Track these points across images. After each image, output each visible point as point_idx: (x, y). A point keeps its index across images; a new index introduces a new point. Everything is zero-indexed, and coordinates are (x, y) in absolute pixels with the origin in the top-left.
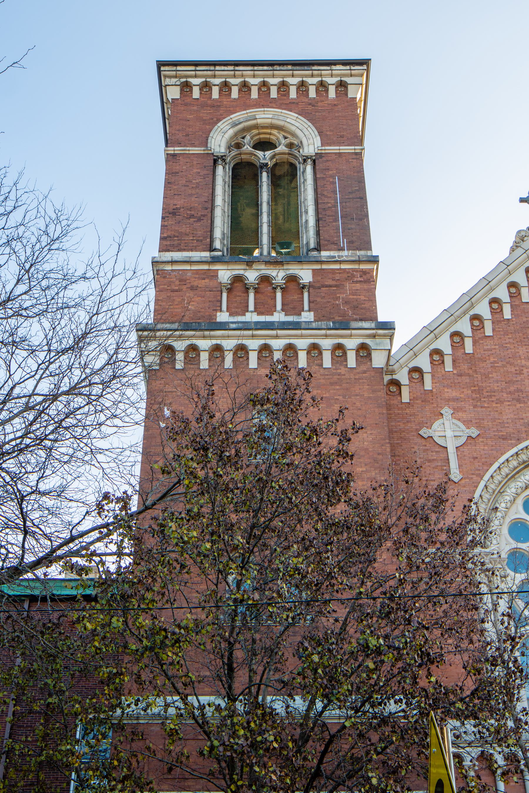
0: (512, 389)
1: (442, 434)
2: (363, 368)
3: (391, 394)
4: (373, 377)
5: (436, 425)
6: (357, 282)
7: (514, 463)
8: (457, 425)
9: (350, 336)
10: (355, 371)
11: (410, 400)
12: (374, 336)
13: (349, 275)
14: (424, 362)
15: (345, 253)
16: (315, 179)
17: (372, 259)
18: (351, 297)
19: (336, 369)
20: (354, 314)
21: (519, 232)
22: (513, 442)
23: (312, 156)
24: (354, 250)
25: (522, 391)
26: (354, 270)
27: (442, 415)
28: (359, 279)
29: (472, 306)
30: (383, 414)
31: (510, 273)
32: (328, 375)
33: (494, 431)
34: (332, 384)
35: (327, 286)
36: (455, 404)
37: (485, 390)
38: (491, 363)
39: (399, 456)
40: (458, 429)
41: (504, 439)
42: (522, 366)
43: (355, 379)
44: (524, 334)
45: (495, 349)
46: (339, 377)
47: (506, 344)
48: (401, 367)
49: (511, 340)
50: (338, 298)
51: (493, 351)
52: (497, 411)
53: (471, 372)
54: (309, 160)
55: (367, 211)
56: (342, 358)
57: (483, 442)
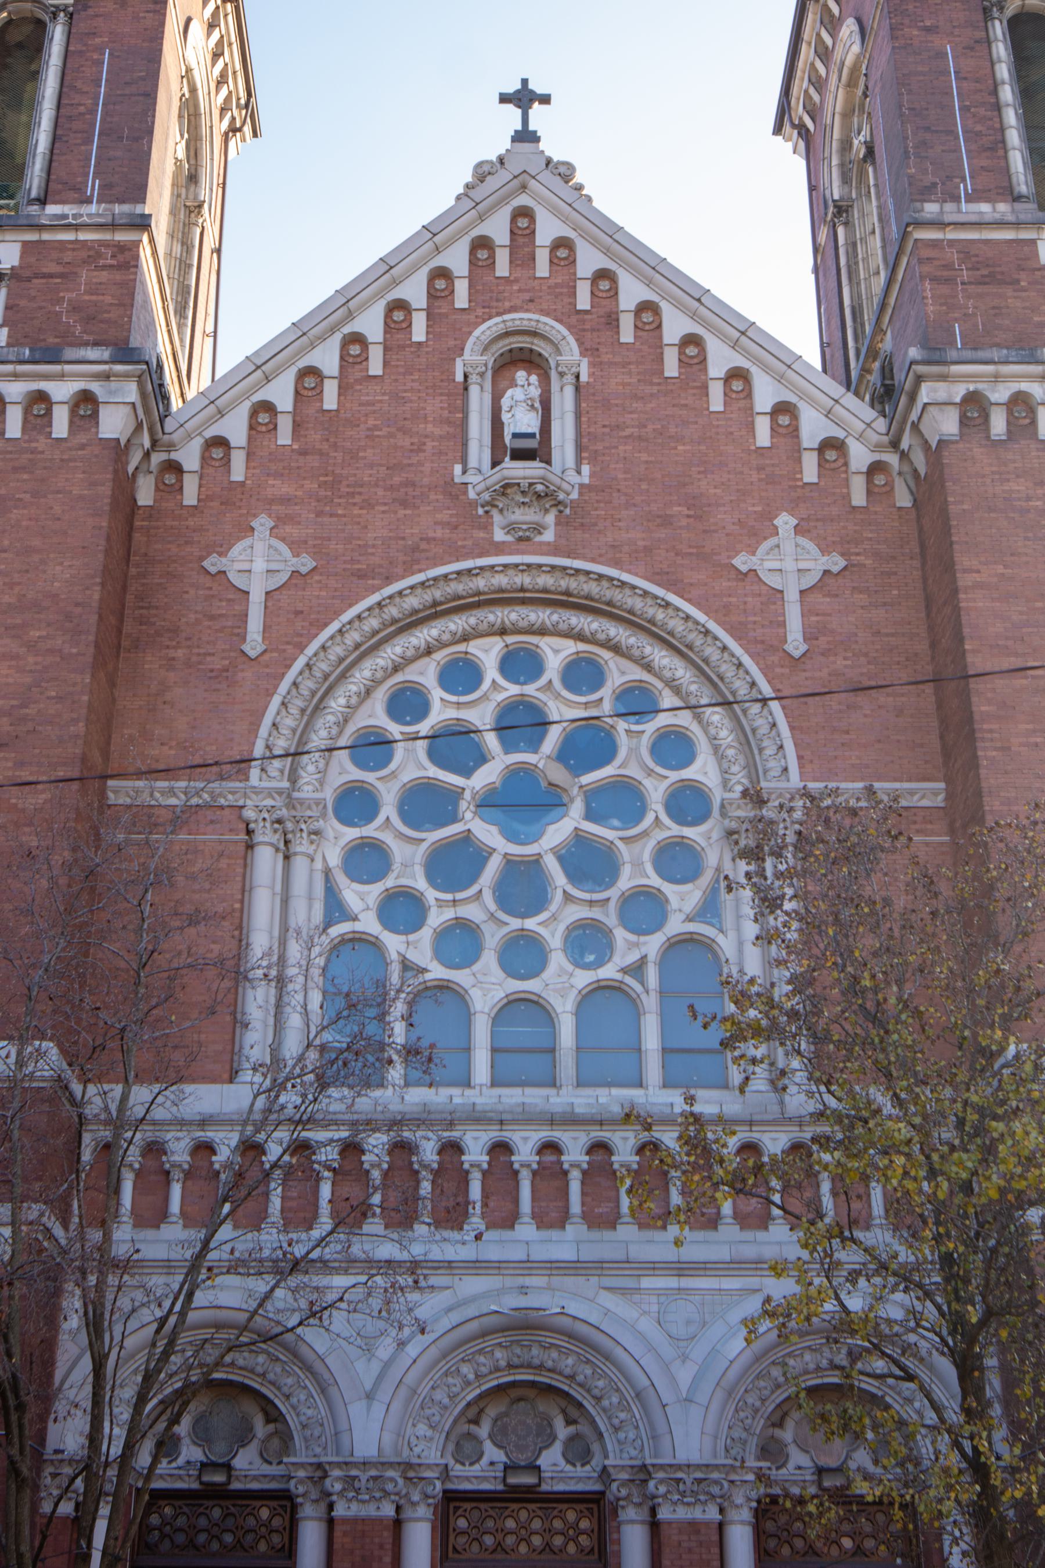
0: (397, 480)
1: (245, 566)
2: (82, 438)
3: (166, 489)
4: (96, 456)
5: (236, 550)
6: (104, 267)
7: (374, 623)
8: (276, 550)
9: (61, 376)
10: (64, 444)
11: (199, 500)
12: (107, 377)
13: (91, 253)
14: (235, 428)
15: (93, 208)
16: (67, 55)
17: (138, 221)
18: (87, 298)
19: (30, 441)
20: (85, 332)
21: (480, 164)
22: (376, 582)
23: (66, 6)
24: (110, 202)
25: (413, 485)
26: (102, 243)
27: (253, 529)
28: (110, 262)
29: (350, 316)
30: (100, 528)
31: (438, 250)
32: (11, 452)
33: (345, 562)
34: (15, 470)
35: (45, 276)
36: (281, 509)
37: (345, 483)
38: (368, 429)
39: (157, 608)
40: (279, 558)
41: (360, 577)
42: (426, 436)
43: (62, 460)
44: (442, 373)
45: (381, 401)
46: (31, 456)
47: (405, 391)
48: (189, 437)
49: (416, 385)
50: (60, 301)
51: (377, 407)
52: (359, 523)
53: (325, 446)
54: (62, 14)
55: (153, 123)
56: (45, 420)
57: (320, 582)
